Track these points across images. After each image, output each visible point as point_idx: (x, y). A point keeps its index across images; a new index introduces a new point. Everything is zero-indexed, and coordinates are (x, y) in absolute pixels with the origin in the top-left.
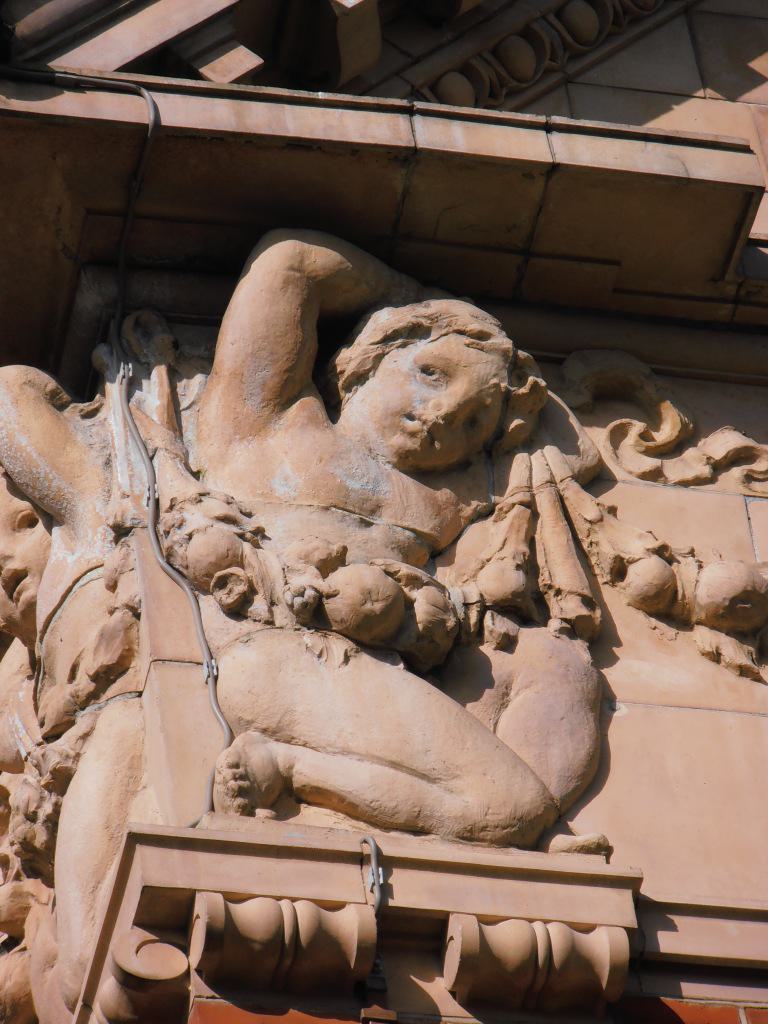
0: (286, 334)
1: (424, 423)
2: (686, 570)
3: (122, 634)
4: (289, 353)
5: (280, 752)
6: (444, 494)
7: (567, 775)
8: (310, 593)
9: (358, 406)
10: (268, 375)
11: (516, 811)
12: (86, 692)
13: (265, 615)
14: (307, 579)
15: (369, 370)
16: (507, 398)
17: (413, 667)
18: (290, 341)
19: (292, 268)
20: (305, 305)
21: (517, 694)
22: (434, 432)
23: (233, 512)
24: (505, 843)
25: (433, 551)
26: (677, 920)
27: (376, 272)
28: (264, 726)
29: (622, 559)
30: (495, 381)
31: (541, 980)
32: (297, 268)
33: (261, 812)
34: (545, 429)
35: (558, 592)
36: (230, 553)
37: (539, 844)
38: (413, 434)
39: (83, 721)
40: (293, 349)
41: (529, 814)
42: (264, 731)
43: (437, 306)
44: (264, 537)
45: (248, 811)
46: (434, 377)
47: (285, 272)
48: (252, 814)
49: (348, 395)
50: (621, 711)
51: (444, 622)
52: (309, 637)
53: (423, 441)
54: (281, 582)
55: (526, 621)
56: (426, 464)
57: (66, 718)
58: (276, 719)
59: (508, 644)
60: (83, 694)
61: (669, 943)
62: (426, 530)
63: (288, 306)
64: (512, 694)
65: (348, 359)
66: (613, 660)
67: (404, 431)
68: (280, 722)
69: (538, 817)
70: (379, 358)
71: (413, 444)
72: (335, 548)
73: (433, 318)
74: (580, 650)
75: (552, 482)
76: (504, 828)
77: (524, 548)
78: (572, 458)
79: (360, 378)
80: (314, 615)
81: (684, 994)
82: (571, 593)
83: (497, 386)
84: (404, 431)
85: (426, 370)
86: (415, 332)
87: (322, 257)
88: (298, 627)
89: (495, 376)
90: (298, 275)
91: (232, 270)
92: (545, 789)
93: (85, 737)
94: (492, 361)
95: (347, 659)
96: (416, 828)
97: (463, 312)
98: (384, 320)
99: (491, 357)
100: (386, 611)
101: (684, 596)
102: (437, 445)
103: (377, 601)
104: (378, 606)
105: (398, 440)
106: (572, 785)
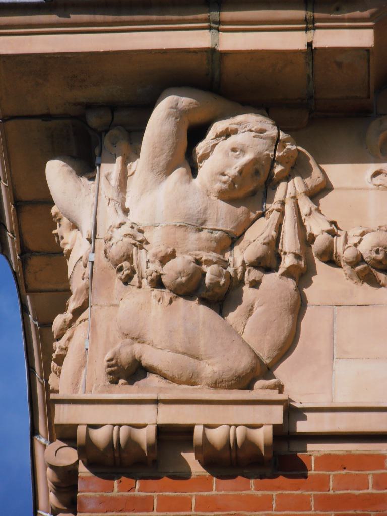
0: (169, 140)
1: (230, 177)
2: (339, 243)
3: (85, 292)
4: (170, 149)
5: (137, 348)
6: (243, 209)
7: (273, 349)
8: (154, 274)
9: (206, 169)
10: (163, 160)
11: (236, 373)
12: (69, 320)
13: (137, 284)
14: (154, 266)
15: (210, 152)
16: (273, 161)
17: (204, 301)
18: (170, 142)
19: (172, 108)
20: (178, 125)
21: (256, 309)
22: (234, 181)
23: (134, 232)
24: (231, 387)
25: (233, 240)
26: (308, 414)
27: (212, 103)
28: (133, 336)
29: (313, 235)
30: (267, 152)
31: (234, 454)
32: (176, 107)
33: (121, 381)
34: (297, 167)
35: (285, 253)
36: (126, 254)
37: (250, 387)
38: (225, 183)
39: (68, 333)
40: (172, 147)
41: (243, 373)
42: (133, 338)
43: (240, 118)
44: (147, 243)
45: (115, 382)
46: (238, 153)
47: (169, 110)
48: (117, 383)
49: (200, 165)
50: (309, 310)
51: (218, 282)
52: (156, 292)
53: (229, 186)
54: (145, 267)
55: (268, 269)
56: (235, 195)
57: (61, 332)
58: (137, 333)
59: (255, 284)
60: (67, 321)
61: (302, 427)
62: (229, 229)
63: (169, 126)
64: (255, 309)
65: (200, 148)
66: (309, 283)
67: (220, 181)
68: (139, 334)
69: (247, 374)
70: (214, 146)
71: (225, 187)
72: (170, 250)
73: (240, 124)
74: (291, 284)
75: (294, 197)
76: (229, 381)
77: (274, 234)
78: (160, 268)
79: (205, 156)
80: (158, 283)
81: (308, 450)
82: (290, 253)
83: (268, 155)
84: (220, 181)
85: (234, 150)
86: (227, 134)
87: (184, 101)
88: (152, 289)
89: (266, 150)
90: (175, 110)
91: (149, 107)
92: (256, 357)
93: (69, 339)
94: (266, 142)
95: (171, 302)
96: (191, 381)
97: (252, 120)
98: (219, 126)
99: (265, 141)
100: (188, 280)
101: (336, 253)
102: (236, 186)
103: (184, 276)
104: (184, 279)
105: (218, 186)
106: (275, 354)
